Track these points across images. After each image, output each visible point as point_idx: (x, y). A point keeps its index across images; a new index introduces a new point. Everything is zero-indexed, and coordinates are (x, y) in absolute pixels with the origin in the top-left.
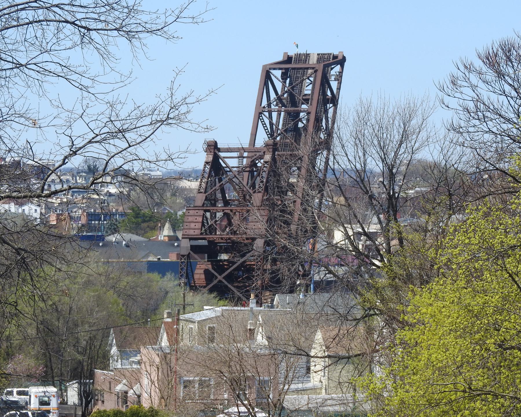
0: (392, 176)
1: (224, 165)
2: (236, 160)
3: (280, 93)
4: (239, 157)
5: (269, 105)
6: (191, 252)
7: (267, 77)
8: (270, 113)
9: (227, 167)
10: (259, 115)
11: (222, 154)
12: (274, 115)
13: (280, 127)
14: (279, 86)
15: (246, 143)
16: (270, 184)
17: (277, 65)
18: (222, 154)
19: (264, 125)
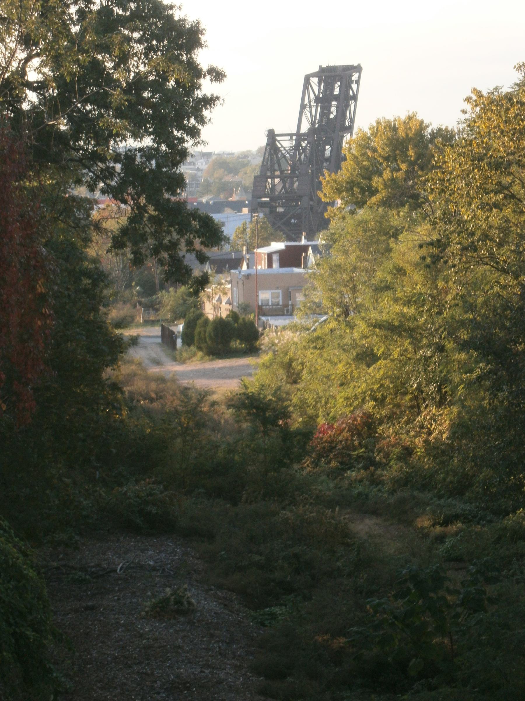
0: (57, 197)
1: (279, 146)
2: (288, 142)
3: (317, 94)
4: (289, 140)
5: (310, 102)
6: (158, 287)
7: (307, 79)
8: (310, 107)
9: (282, 147)
10: (303, 107)
11: (278, 138)
12: (314, 109)
13: (318, 118)
14: (316, 89)
15: (295, 131)
16: (143, 556)
17: (313, 75)
18: (278, 138)
19: (306, 117)
